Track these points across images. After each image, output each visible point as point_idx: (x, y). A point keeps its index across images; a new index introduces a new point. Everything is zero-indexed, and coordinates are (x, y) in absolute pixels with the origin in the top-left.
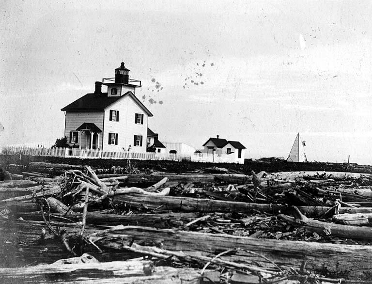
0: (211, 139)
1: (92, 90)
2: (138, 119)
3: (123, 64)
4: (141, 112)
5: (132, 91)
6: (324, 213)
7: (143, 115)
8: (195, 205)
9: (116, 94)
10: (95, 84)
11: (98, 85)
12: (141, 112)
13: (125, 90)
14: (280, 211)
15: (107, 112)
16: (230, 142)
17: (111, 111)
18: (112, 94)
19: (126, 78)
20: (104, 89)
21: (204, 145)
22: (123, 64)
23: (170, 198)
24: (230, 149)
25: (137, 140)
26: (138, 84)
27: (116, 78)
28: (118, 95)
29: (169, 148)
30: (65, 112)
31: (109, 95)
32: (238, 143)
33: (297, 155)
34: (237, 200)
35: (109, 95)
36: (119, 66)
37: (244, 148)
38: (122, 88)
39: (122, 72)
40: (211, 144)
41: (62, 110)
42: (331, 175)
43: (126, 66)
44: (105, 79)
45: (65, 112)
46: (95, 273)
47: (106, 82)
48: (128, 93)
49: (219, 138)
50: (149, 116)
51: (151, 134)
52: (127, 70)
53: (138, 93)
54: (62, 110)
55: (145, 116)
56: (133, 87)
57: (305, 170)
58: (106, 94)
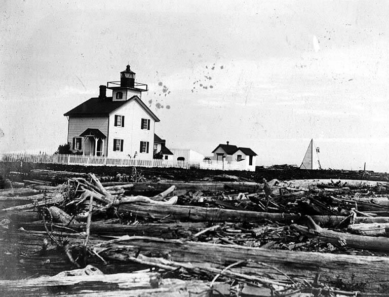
0: (221, 146)
1: (96, 94)
2: (145, 124)
3: (128, 67)
4: (147, 117)
5: (139, 95)
7: (149, 120)
10: (99, 88)
11: (103, 89)
12: (147, 117)
13: (130, 94)
15: (112, 117)
16: (241, 149)
17: (116, 116)
19: (132, 81)
20: (109, 93)
21: (213, 152)
22: (128, 67)
24: (241, 156)
25: (144, 146)
28: (124, 99)
29: (177, 155)
30: (68, 117)
31: (114, 99)
32: (249, 149)
33: (310, 162)
35: (114, 99)
36: (124, 69)
37: (255, 155)
39: (127, 76)
40: (220, 151)
41: (65, 115)
43: (132, 69)
44: (110, 83)
45: (68, 117)
47: (110, 85)
49: (229, 144)
51: (157, 140)
52: (133, 74)
53: (144, 97)
54: (65, 115)
55: (152, 121)
56: (139, 91)
57: (319, 178)
58: (111, 98)
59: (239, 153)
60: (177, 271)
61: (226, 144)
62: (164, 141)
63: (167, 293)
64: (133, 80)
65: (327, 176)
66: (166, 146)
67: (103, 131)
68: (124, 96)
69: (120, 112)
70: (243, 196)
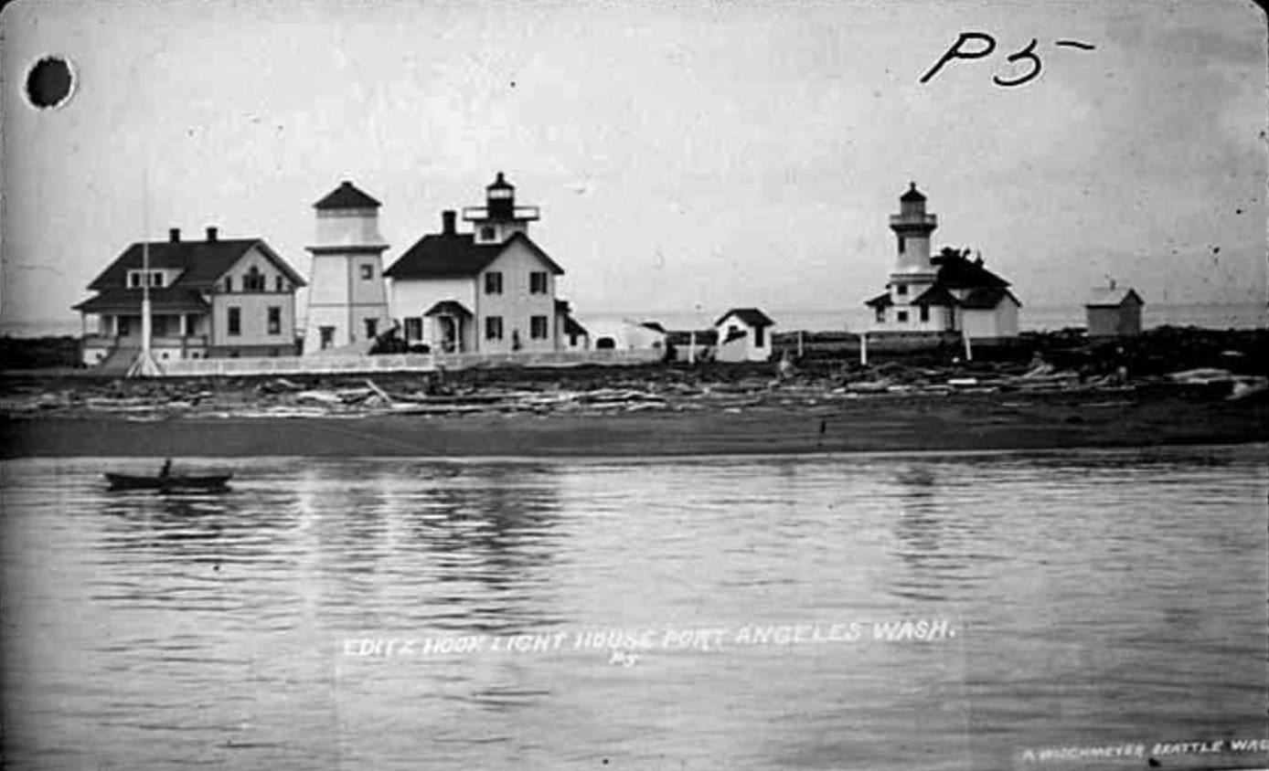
1: (438, 228)
2: (538, 284)
3: (500, 176)
4: (539, 268)
6: (610, 656)
7: (545, 274)
10: (337, 185)
11: (449, 217)
12: (539, 268)
14: (1121, 350)
20: (462, 228)
22: (500, 176)
25: (538, 325)
27: (488, 209)
29: (595, 335)
31: (478, 240)
32: (755, 312)
34: (462, 466)
35: (478, 240)
36: (493, 180)
43: (507, 179)
46: (1063, 350)
52: (511, 188)
56: (524, 221)
58: (470, 237)
60: (1076, 335)
63: (360, 696)
64: (510, 201)
65: (130, 257)
70: (470, 503)
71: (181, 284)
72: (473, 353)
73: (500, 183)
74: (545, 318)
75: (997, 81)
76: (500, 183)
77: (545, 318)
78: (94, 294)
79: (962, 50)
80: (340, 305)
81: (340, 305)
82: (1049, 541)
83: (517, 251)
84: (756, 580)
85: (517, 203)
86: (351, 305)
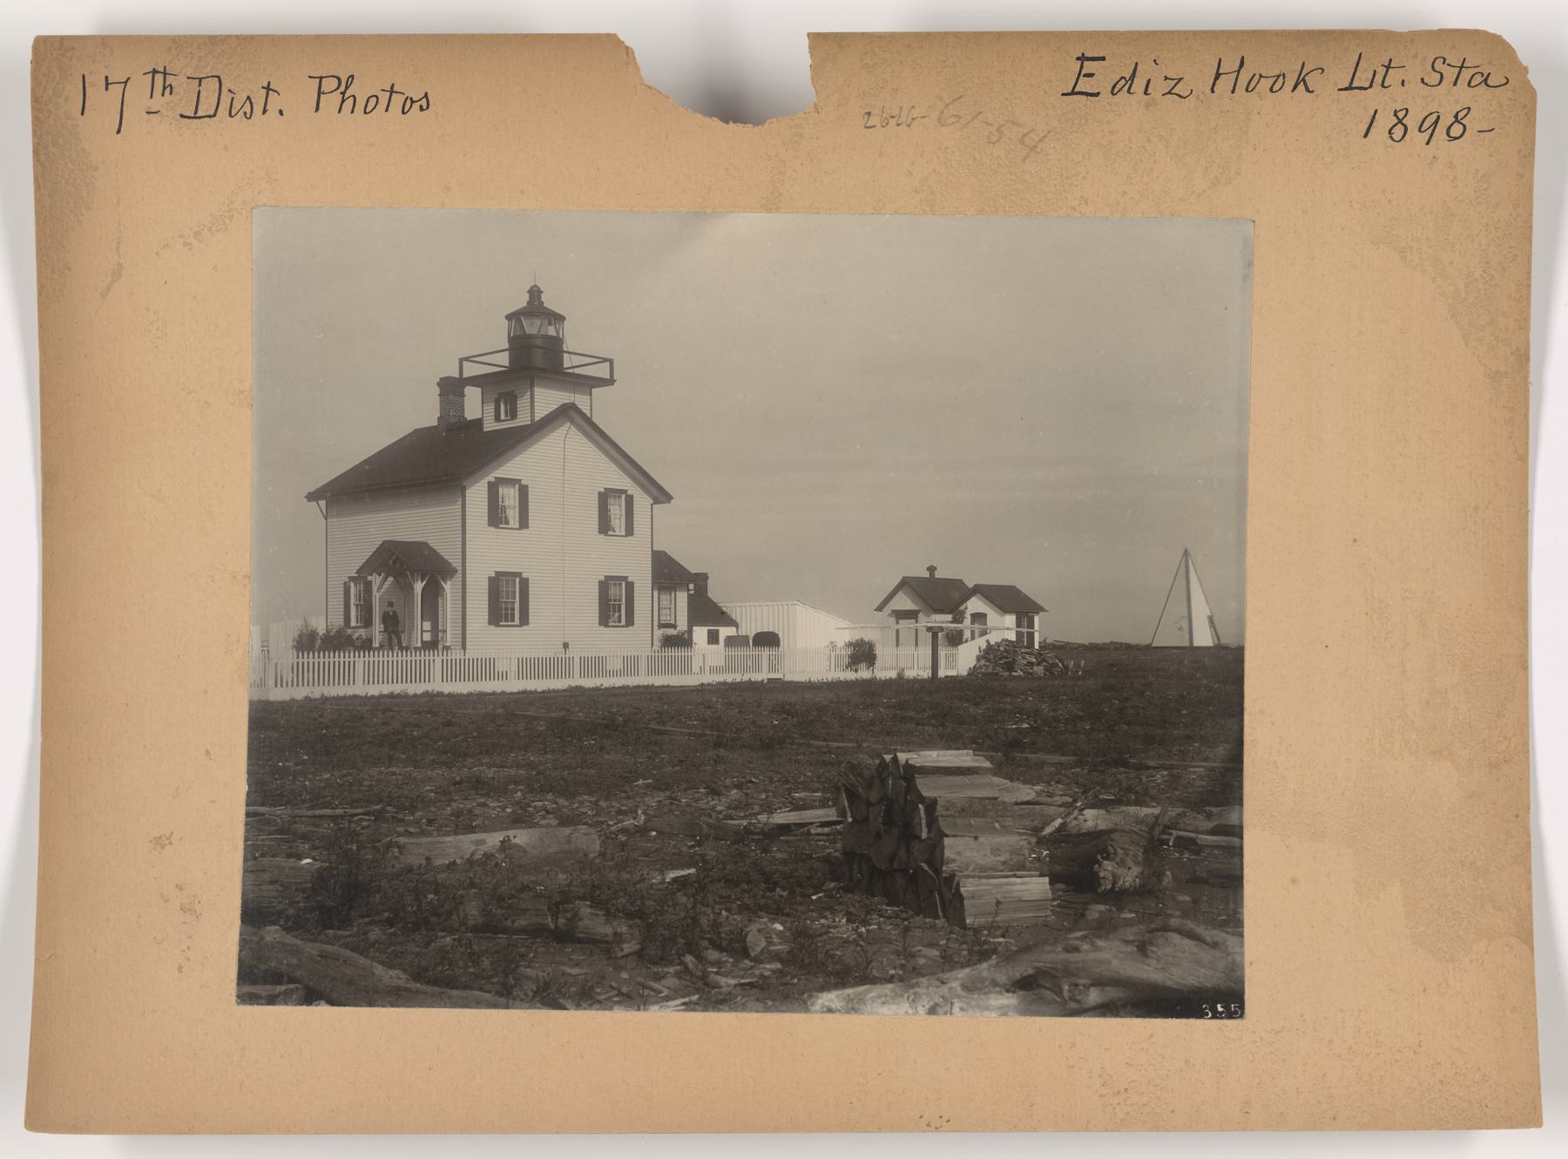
0: (905, 584)
1: (425, 413)
3: (535, 293)
5: (582, 401)
8: (551, 918)
9: (513, 414)
11: (451, 389)
12: (619, 480)
13: (546, 399)
15: (477, 494)
16: (978, 590)
17: (493, 488)
18: (497, 418)
19: (554, 347)
20: (474, 405)
21: (880, 608)
22: (535, 293)
23: (1015, 884)
24: (984, 616)
26: (601, 371)
28: (523, 419)
30: (323, 503)
33: (1185, 625)
35: (490, 425)
36: (522, 301)
37: (1038, 609)
38: (536, 389)
39: (532, 327)
40: (904, 602)
41: (313, 497)
42: (856, 671)
43: (549, 301)
44: (467, 359)
45: (323, 503)
47: (471, 370)
48: (566, 412)
49: (938, 575)
50: (656, 501)
51: (668, 574)
53: (598, 404)
54: (313, 497)
55: (642, 501)
56: (588, 384)
57: (350, 596)
58: (478, 423)
59: (975, 605)
61: (927, 574)
62: (509, 317)
66: (709, 595)
67: (448, 551)
68: (523, 404)
69: (518, 466)
71: (1222, 750)
72: (456, 655)
73: (535, 307)
74: (709, 630)
75: (1422, 80)
76: (535, 307)
77: (709, 630)
78: (962, 608)
79: (1173, 91)
80: (1396, 124)
81: (1396, 124)
82: (1067, 998)
83: (565, 440)
84: (542, 830)
85: (569, 345)
86: (392, 92)
